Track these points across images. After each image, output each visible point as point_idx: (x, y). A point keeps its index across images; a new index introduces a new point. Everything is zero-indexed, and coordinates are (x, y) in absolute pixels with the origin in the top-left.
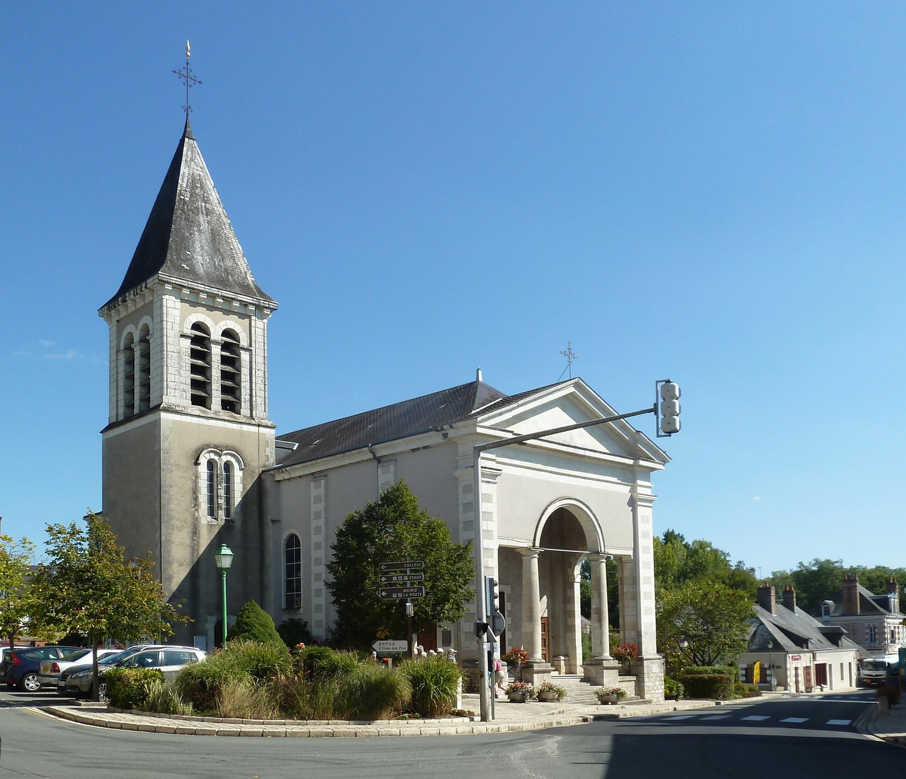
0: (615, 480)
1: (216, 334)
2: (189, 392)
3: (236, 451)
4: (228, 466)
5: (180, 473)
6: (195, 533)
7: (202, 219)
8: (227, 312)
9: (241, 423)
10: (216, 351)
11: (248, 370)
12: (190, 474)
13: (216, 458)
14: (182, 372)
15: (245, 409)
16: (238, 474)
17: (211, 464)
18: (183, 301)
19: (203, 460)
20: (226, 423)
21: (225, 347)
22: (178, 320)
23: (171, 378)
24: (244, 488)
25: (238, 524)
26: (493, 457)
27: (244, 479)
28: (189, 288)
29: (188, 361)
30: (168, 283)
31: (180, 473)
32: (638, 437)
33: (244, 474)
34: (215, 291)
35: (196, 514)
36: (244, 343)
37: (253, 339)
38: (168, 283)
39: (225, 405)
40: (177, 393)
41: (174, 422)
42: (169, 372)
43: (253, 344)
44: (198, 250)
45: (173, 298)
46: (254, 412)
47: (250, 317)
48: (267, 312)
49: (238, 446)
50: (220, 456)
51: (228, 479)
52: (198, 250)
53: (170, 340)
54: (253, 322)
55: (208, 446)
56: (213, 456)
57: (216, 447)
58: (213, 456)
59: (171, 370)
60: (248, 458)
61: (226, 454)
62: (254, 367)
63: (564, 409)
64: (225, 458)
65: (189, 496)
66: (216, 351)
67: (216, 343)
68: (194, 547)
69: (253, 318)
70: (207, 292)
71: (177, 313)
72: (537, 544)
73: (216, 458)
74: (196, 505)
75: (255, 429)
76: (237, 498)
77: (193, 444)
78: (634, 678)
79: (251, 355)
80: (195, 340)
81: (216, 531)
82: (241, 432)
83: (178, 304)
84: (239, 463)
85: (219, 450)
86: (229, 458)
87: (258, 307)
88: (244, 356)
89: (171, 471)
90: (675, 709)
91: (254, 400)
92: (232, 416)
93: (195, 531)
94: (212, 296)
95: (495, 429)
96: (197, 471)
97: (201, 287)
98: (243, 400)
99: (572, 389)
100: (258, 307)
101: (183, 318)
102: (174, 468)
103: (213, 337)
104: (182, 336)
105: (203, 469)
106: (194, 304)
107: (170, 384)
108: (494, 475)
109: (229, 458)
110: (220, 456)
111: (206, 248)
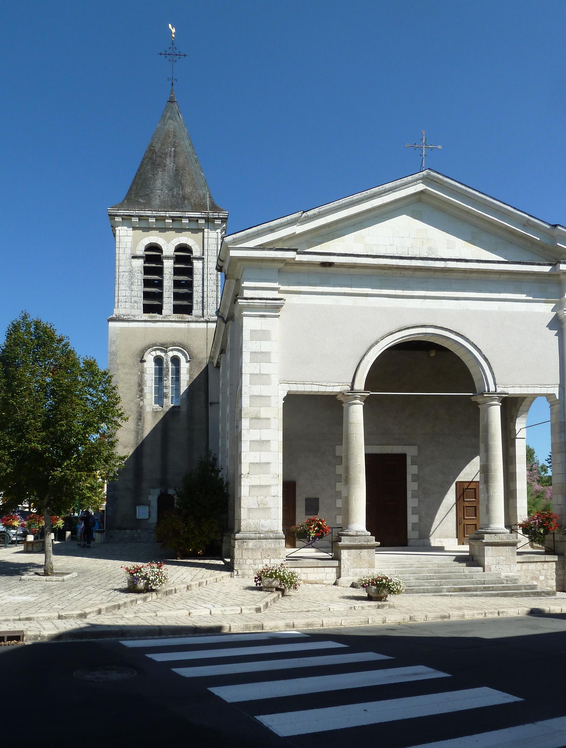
0: (523, 297)
1: (168, 250)
2: (141, 302)
3: (183, 347)
4: (176, 361)
5: (126, 370)
6: (140, 419)
7: (169, 162)
8: (180, 230)
9: (189, 322)
10: (168, 265)
11: (201, 276)
12: (136, 371)
13: (162, 354)
14: (134, 287)
15: (197, 310)
16: (184, 366)
17: (158, 361)
18: (134, 228)
19: (150, 358)
20: (173, 324)
21: (178, 260)
22: (129, 245)
23: (122, 293)
24: (190, 378)
25: (184, 410)
26: (275, 285)
27: (190, 370)
28: (137, 216)
29: (140, 277)
30: (117, 216)
31: (126, 370)
32: (555, 232)
33: (190, 366)
34: (162, 214)
35: (141, 403)
36: (196, 253)
37: (206, 248)
38: (117, 216)
39: (177, 309)
40: (128, 305)
41: (121, 328)
42: (121, 288)
43: (206, 253)
44: (159, 185)
45: (126, 228)
46: (205, 311)
47: (203, 230)
48: (218, 222)
49: (185, 342)
50: (166, 352)
51: (177, 372)
52: (159, 185)
53: (122, 263)
54: (206, 234)
55: (155, 345)
56: (159, 353)
57: (162, 345)
58: (159, 353)
59: (122, 287)
60: (195, 351)
61: (172, 350)
62: (205, 272)
63: (416, 215)
64: (171, 354)
65: (135, 388)
66: (168, 265)
67: (168, 258)
68: (138, 431)
69: (206, 230)
70: (154, 217)
71: (129, 239)
72: (360, 385)
73: (162, 354)
74: (141, 396)
75: (204, 325)
76: (184, 387)
77: (140, 344)
78: (556, 558)
79: (203, 263)
80: (148, 259)
81: (161, 416)
82: (189, 330)
83: (130, 232)
84: (186, 356)
85: (164, 347)
86: (176, 353)
87: (207, 220)
88: (197, 265)
89: (118, 370)
90: (65, 628)
91: (205, 300)
92: (182, 318)
93: (140, 417)
94: (159, 219)
95: (263, 249)
96: (143, 367)
97: (149, 213)
98: (195, 302)
99: (421, 187)
100: (207, 220)
101: (135, 243)
102: (120, 367)
103: (165, 253)
104: (134, 257)
105: (150, 366)
106: (147, 229)
107: (121, 298)
108: (274, 307)
109: (176, 353)
110: (166, 352)
111: (167, 182)
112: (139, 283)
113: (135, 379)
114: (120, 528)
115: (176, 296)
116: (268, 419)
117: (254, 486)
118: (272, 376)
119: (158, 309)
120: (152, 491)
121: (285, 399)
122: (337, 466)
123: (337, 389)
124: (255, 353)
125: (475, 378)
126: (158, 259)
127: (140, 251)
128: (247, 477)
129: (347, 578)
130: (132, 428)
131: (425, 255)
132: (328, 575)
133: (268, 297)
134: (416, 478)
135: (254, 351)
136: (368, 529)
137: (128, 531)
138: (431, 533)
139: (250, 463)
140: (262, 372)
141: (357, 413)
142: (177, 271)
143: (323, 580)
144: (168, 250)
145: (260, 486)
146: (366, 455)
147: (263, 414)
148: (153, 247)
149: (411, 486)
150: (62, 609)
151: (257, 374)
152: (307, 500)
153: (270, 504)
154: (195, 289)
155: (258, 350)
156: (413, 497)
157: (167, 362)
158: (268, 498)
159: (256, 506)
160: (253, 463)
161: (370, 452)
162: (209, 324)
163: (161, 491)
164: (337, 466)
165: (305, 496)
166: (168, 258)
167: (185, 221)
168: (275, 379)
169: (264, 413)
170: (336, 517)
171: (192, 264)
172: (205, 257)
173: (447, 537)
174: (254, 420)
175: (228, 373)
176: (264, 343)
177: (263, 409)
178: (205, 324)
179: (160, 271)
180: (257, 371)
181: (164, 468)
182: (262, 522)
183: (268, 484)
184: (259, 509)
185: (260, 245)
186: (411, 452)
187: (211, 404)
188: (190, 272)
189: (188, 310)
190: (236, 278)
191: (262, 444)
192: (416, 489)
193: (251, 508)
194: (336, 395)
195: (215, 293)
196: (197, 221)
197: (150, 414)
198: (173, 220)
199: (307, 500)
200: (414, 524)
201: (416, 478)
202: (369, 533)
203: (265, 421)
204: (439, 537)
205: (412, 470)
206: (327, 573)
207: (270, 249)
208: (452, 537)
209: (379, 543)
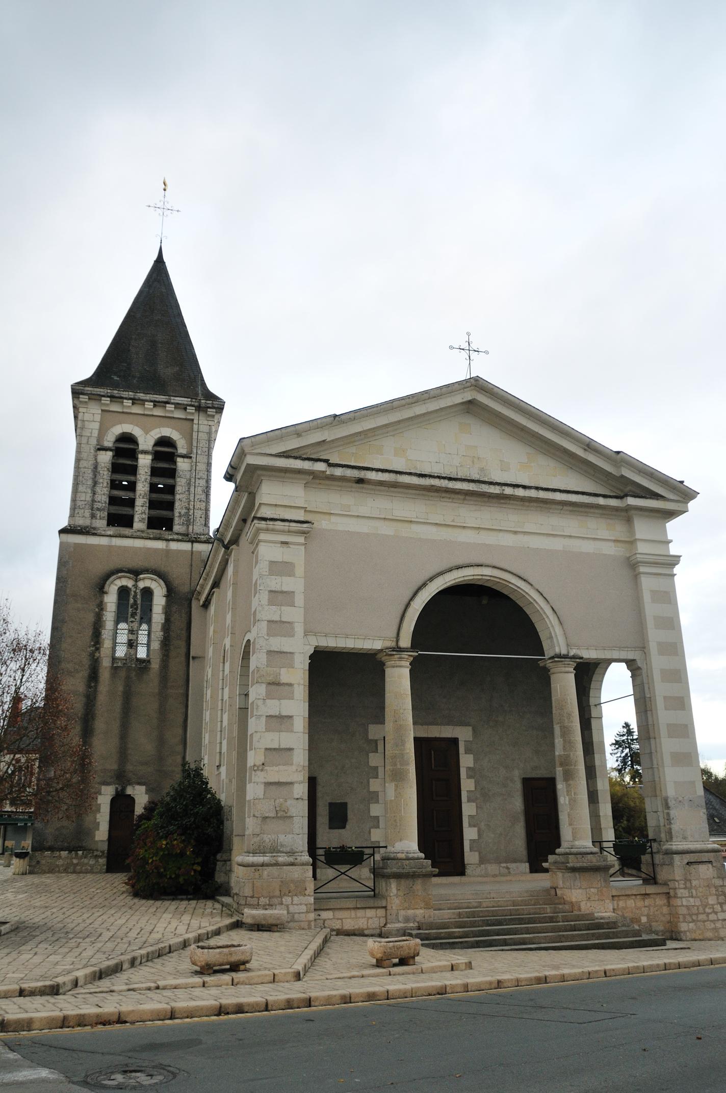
1: (146, 441)
10: (144, 462)
17: (123, 592)
22: (95, 433)
36: (182, 449)
65: (89, 632)
66: (144, 462)
67: (145, 452)
72: (406, 641)
77: (98, 568)
82: (168, 552)
88: (182, 465)
95: (288, 457)
101: (102, 431)
103: (141, 447)
112: (105, 484)
113: (91, 618)
114: (51, 849)
115: (152, 505)
116: (291, 685)
117: (271, 784)
118: (296, 624)
119: (128, 522)
120: (103, 788)
121: (311, 657)
122: (371, 755)
123: (377, 645)
124: (275, 592)
125: (543, 636)
126: (132, 454)
127: (109, 441)
128: (262, 770)
129: (397, 925)
130: (81, 690)
131: (476, 476)
132: (370, 921)
133: (286, 518)
134: (472, 773)
135: (274, 589)
136: (421, 848)
137: (64, 854)
138: (336, 867)
139: (266, 749)
140: (283, 620)
141: (399, 680)
142: (154, 472)
143: (363, 930)
144: (146, 441)
145: (279, 784)
146: (416, 739)
147: (284, 679)
148: (127, 439)
149: (467, 785)
150: (22, 979)
151: (276, 622)
152: (331, 804)
153: (293, 812)
154: (178, 497)
155: (278, 588)
156: (469, 800)
157: (135, 596)
158: (289, 802)
159: (272, 814)
160: (270, 749)
161: (418, 735)
162: (195, 545)
163: (117, 789)
164: (371, 755)
165: (329, 800)
166: (145, 452)
167: (170, 407)
168: (299, 629)
169: (285, 676)
170: (370, 833)
171: (175, 463)
172: (194, 456)
173: (515, 861)
174: (273, 687)
175: (229, 617)
176: (286, 579)
177: (283, 671)
178: (189, 544)
179: (133, 470)
180: (276, 618)
181: (123, 754)
182: (282, 838)
183: (289, 780)
184: (277, 817)
185: (284, 452)
186: (463, 734)
187: (194, 658)
188: (172, 473)
189: (167, 524)
190: (249, 490)
191: (280, 721)
192: (473, 789)
193: (267, 817)
194: (375, 654)
195: (204, 504)
196: (185, 409)
197: (108, 670)
198: (155, 406)
199: (331, 804)
200: (472, 841)
201: (472, 773)
202: (422, 855)
203: (287, 688)
204: (506, 862)
205: (466, 761)
206: (368, 918)
207: (296, 458)
208: (521, 861)
209: (437, 870)
